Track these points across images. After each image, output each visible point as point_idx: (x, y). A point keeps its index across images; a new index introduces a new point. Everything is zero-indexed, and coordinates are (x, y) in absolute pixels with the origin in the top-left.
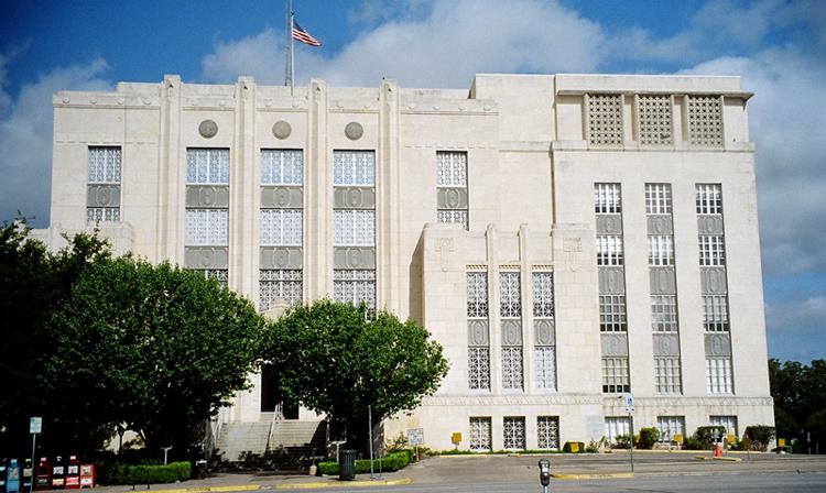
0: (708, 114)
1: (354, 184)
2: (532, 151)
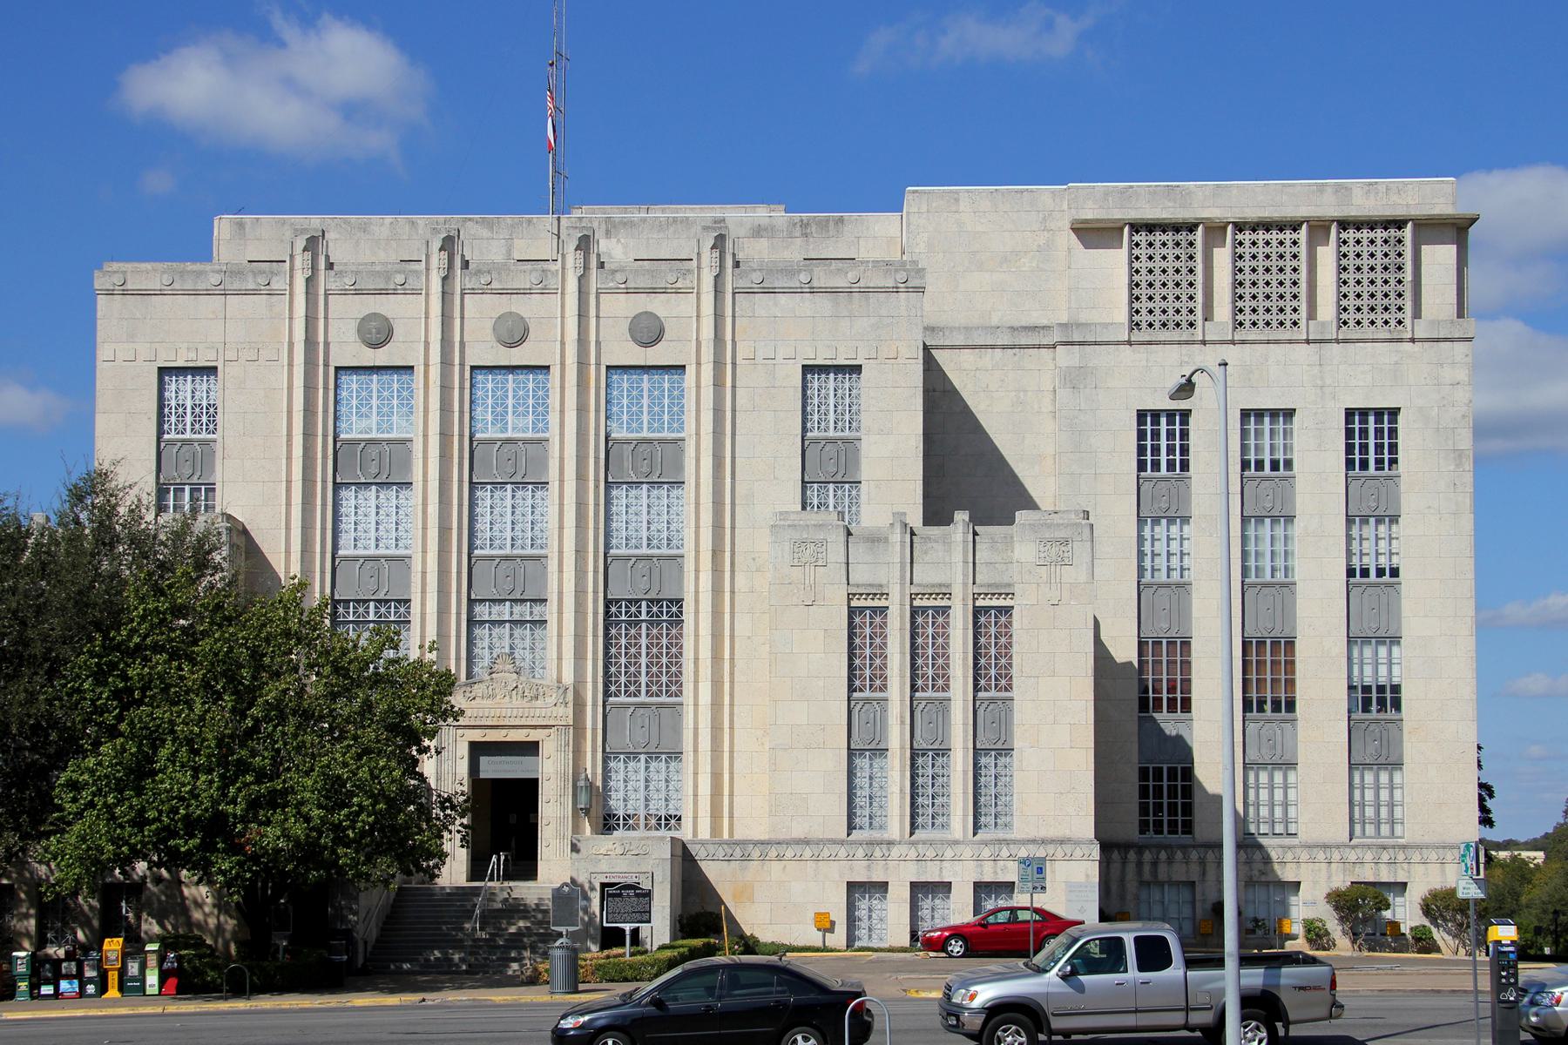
0: (1379, 261)
1: (645, 434)
2: (1013, 347)
